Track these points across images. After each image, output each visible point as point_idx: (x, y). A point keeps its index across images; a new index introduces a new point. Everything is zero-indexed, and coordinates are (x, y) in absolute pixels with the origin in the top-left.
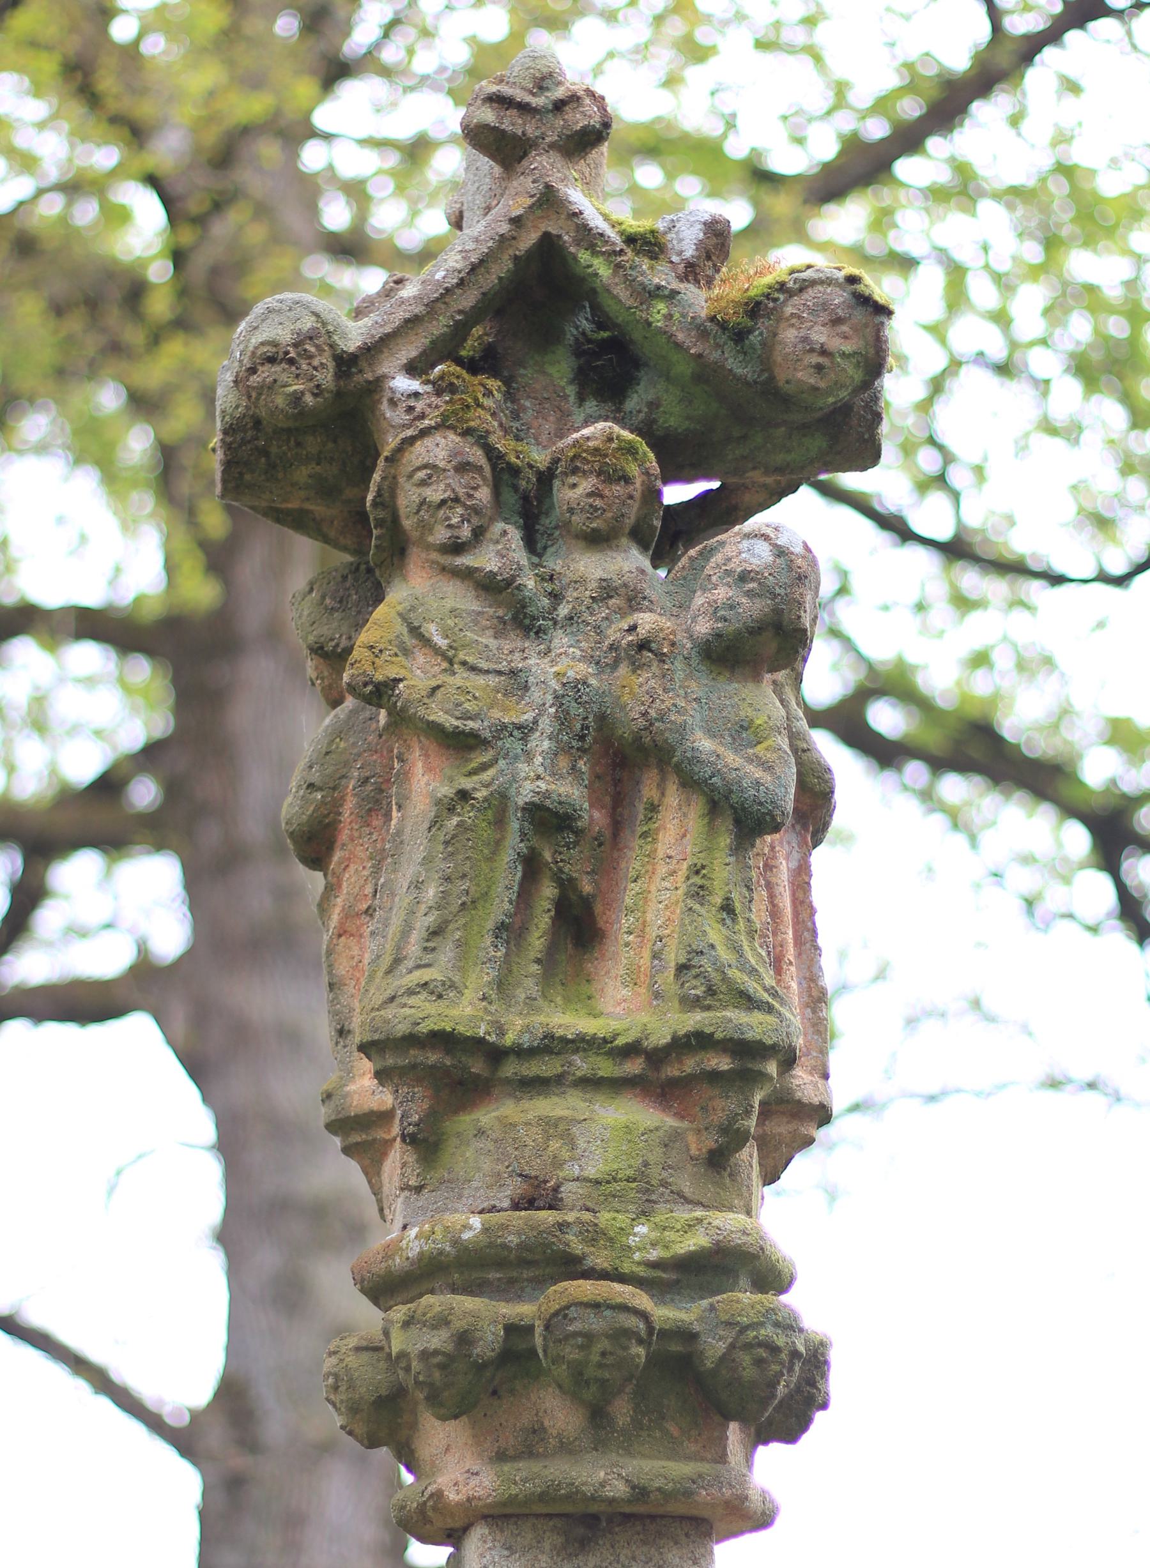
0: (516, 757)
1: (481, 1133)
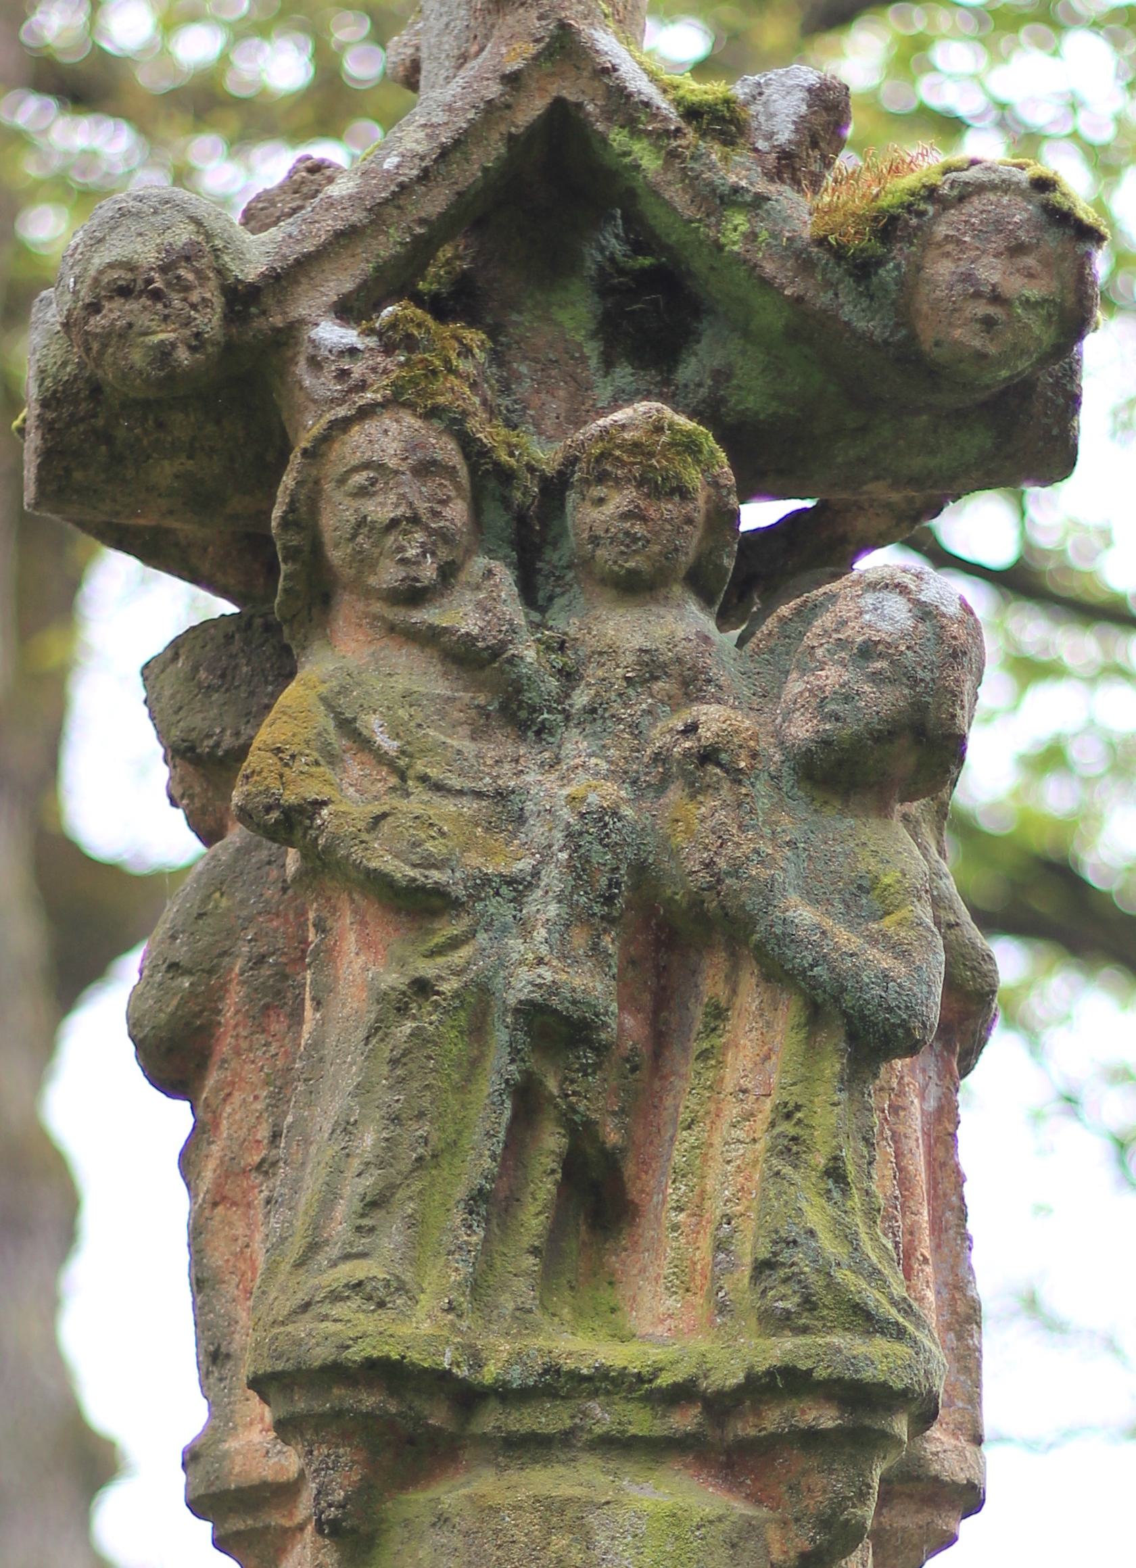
0: (505, 929)
1: (442, 1520)
